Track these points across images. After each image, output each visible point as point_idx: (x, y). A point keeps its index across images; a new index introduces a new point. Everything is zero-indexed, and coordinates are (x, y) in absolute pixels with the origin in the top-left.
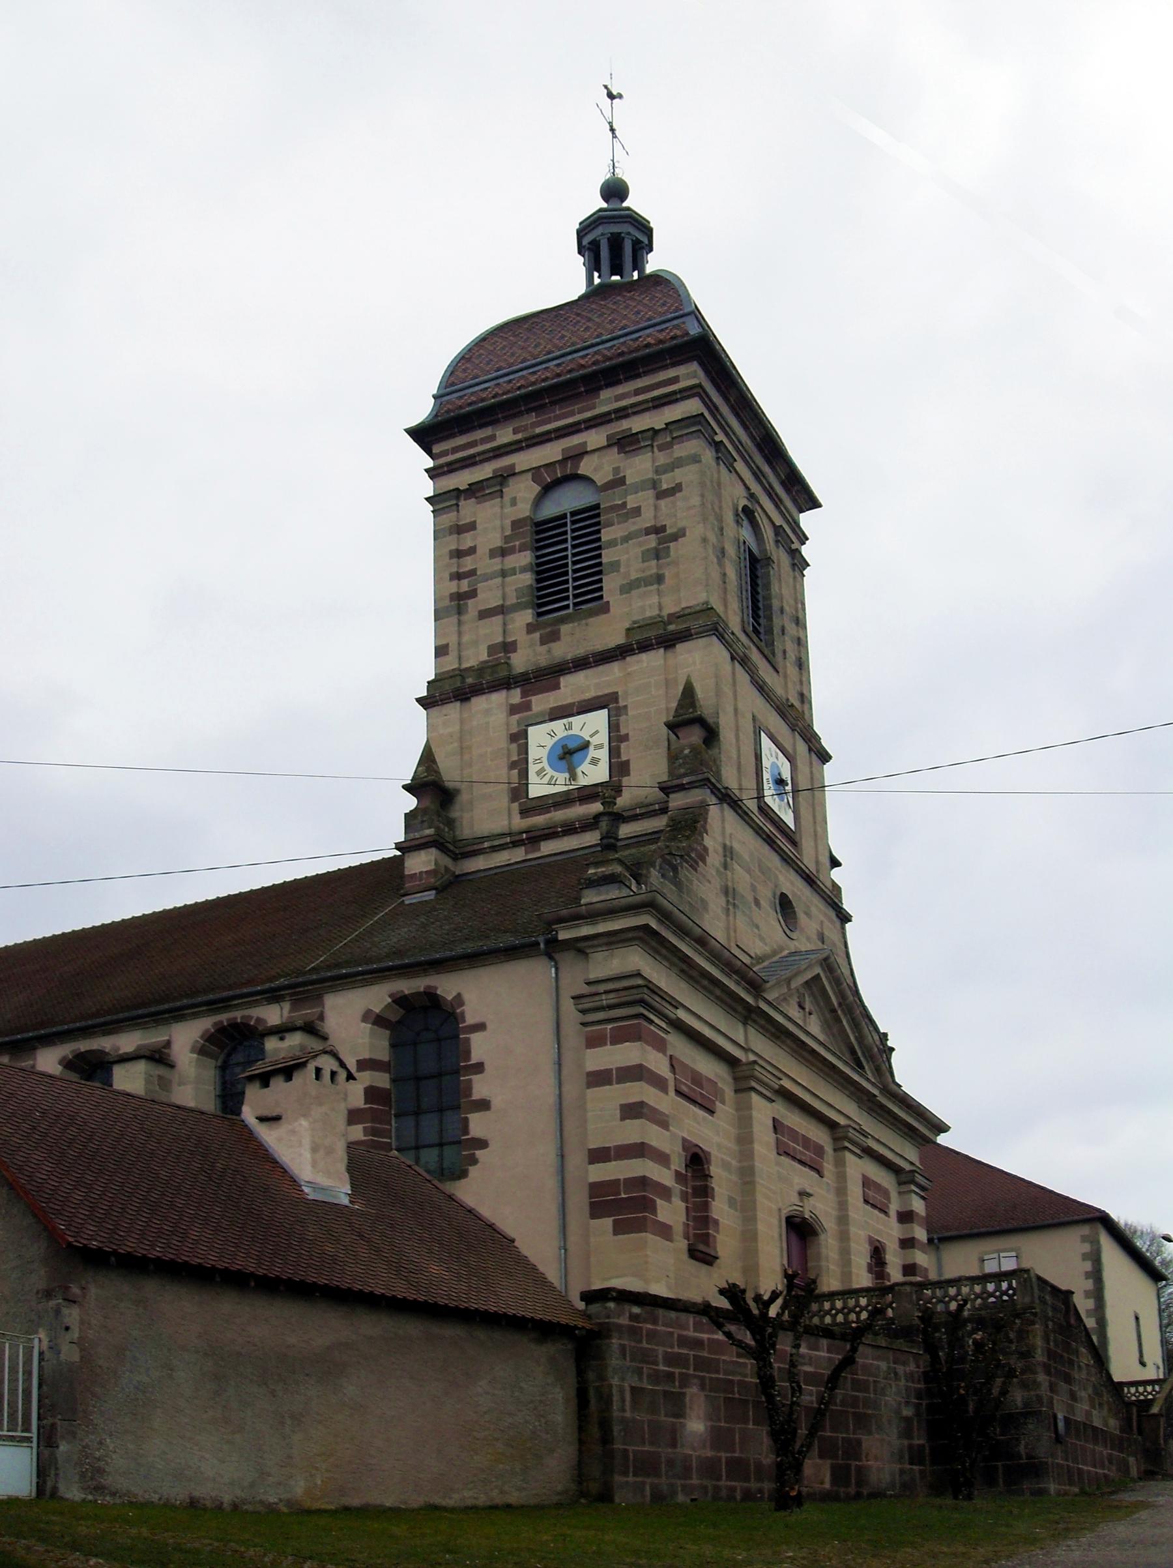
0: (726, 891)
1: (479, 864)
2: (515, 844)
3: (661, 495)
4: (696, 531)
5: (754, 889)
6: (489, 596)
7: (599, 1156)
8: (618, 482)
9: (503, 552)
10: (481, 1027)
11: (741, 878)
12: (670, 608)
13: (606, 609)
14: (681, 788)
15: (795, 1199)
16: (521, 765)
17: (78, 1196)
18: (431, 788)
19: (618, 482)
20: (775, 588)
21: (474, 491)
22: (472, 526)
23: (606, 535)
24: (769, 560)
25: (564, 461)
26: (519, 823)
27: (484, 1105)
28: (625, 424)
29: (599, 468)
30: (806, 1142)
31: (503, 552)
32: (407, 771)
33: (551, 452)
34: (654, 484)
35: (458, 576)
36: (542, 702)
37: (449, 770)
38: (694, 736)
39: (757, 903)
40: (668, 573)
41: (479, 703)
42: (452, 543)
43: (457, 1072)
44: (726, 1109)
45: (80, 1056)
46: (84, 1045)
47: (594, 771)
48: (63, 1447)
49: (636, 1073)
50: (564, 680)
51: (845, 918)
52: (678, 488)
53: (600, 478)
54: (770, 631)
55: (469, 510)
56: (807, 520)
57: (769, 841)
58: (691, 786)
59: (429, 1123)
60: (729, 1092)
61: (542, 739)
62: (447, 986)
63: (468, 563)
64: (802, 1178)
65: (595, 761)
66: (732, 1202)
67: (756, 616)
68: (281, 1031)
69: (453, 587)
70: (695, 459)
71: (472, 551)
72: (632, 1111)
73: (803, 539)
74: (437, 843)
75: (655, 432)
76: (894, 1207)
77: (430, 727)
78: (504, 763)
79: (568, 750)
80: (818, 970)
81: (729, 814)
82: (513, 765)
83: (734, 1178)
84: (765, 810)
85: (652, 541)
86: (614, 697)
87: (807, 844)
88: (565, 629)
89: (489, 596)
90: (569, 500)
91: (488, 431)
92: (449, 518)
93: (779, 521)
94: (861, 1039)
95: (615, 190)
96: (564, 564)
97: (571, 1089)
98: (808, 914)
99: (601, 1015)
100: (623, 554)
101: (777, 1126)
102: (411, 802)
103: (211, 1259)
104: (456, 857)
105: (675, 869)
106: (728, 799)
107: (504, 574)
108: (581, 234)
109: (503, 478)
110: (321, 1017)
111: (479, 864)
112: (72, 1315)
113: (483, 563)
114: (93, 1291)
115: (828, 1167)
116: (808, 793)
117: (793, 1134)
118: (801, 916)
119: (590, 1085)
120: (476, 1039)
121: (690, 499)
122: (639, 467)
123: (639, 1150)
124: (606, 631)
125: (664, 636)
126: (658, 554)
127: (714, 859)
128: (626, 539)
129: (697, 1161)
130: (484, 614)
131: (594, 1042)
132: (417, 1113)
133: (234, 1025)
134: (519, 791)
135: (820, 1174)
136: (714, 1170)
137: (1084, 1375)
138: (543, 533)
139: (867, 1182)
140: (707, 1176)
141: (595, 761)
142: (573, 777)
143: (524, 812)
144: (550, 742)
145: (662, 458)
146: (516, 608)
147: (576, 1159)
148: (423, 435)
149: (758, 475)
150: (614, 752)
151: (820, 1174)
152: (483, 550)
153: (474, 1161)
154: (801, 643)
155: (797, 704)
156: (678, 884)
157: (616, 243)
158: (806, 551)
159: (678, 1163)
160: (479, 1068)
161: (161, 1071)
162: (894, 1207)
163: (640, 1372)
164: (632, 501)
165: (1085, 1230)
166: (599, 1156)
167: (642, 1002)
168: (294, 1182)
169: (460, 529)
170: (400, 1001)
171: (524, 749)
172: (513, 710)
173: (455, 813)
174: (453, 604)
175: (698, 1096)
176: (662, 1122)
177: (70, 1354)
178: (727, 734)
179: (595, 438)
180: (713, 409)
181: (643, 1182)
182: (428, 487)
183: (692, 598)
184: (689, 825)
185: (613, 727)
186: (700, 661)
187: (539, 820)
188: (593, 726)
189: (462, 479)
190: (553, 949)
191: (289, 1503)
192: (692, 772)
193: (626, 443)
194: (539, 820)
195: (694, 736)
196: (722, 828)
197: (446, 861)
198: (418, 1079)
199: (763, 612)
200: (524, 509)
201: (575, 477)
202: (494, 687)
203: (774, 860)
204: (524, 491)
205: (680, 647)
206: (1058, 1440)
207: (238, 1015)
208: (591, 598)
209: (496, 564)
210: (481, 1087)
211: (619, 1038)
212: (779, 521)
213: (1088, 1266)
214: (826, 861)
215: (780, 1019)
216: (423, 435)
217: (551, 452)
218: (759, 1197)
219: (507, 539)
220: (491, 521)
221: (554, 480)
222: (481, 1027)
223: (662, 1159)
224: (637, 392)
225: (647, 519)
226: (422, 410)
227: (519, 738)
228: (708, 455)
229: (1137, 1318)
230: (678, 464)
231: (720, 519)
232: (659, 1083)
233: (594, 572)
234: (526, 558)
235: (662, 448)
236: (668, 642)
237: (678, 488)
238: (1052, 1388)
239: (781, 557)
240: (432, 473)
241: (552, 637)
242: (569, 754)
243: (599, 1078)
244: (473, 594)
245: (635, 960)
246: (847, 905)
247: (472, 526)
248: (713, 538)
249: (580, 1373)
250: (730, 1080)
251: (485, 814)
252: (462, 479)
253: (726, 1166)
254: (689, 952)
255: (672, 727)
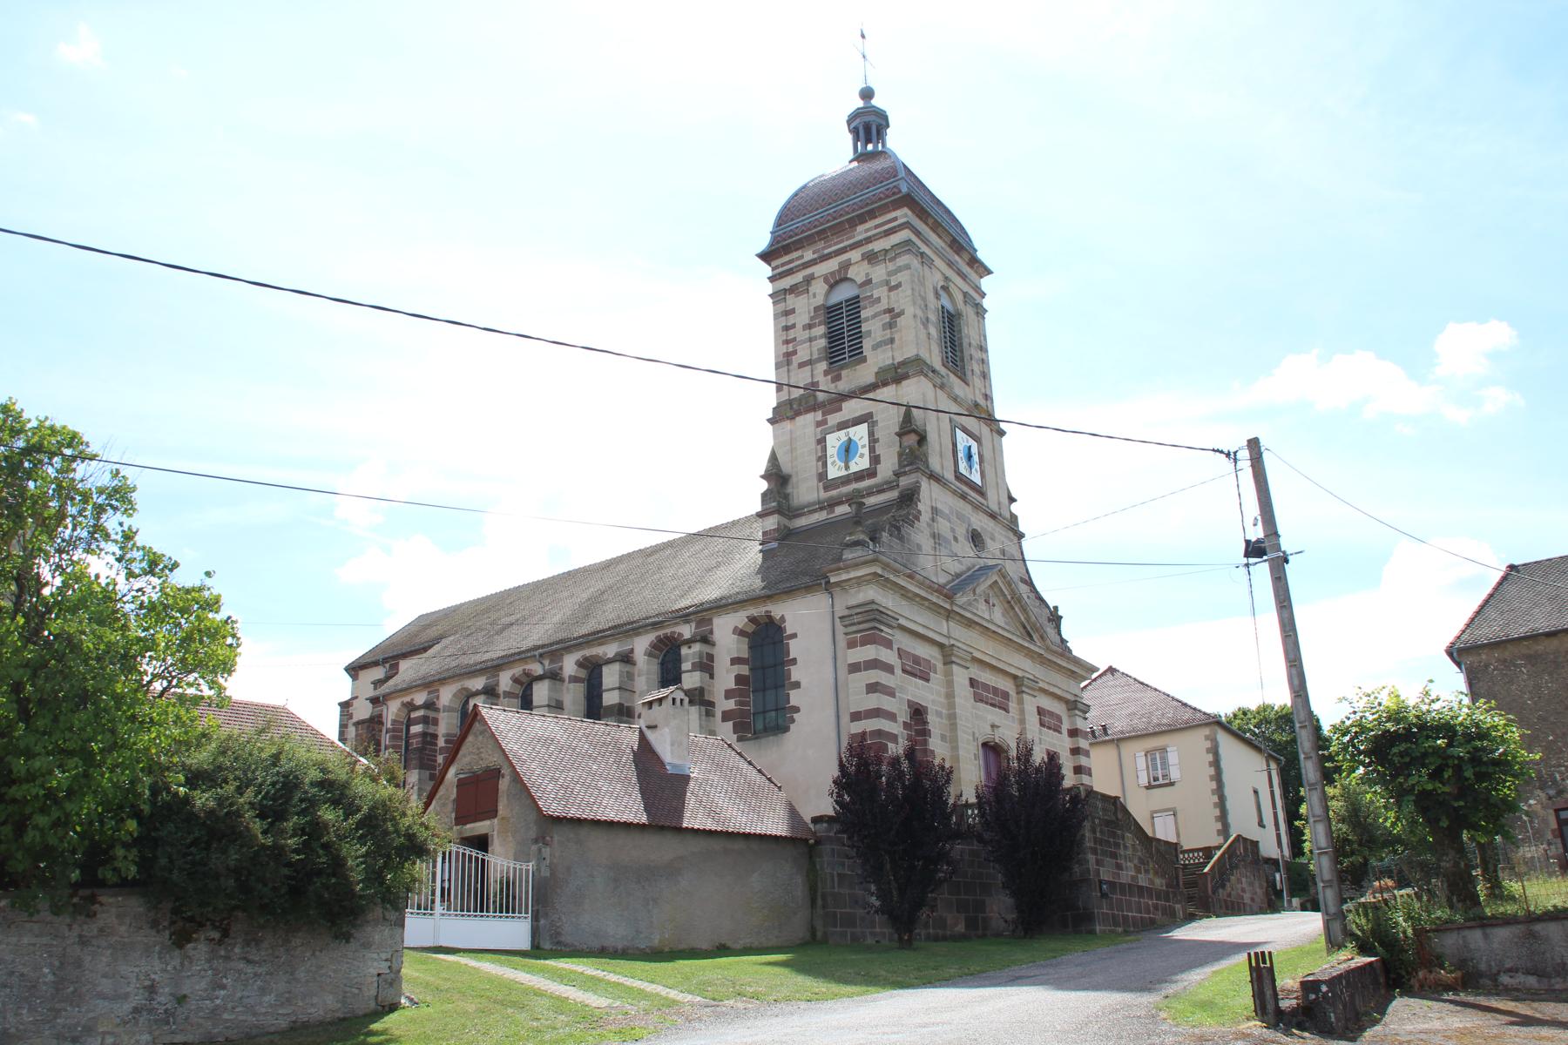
0: (934, 536)
1: (802, 522)
2: (821, 509)
3: (892, 289)
4: (910, 311)
5: (953, 530)
6: (803, 354)
7: (856, 717)
8: (868, 282)
9: (809, 327)
10: (794, 636)
11: (943, 526)
12: (899, 359)
13: (864, 360)
14: (905, 473)
15: (988, 730)
16: (823, 459)
17: (550, 787)
18: (777, 477)
19: (868, 282)
20: (965, 331)
21: (793, 290)
22: (793, 311)
23: (864, 314)
24: (959, 315)
25: (839, 271)
26: (823, 495)
27: (797, 685)
28: (870, 247)
29: (858, 273)
30: (995, 691)
31: (809, 327)
32: (762, 465)
33: (832, 265)
34: (887, 283)
35: (787, 342)
36: (834, 419)
37: (786, 468)
38: (911, 440)
39: (956, 539)
40: (896, 337)
41: (800, 420)
42: (783, 322)
43: (783, 664)
44: (937, 677)
45: (586, 659)
46: (588, 652)
47: (861, 463)
48: (542, 922)
49: (874, 664)
50: (845, 405)
51: (1021, 536)
52: (899, 285)
53: (860, 280)
54: (962, 360)
55: (792, 301)
56: (985, 283)
57: (964, 497)
58: (911, 472)
59: (770, 694)
60: (940, 666)
61: (834, 441)
62: (777, 610)
63: (792, 334)
64: (994, 715)
65: (862, 456)
66: (943, 738)
67: (954, 350)
68: (689, 642)
69: (784, 349)
70: (908, 267)
71: (794, 326)
72: (873, 688)
73: (983, 295)
74: (778, 511)
75: (886, 251)
76: (1065, 727)
77: (775, 437)
78: (814, 458)
79: (851, 450)
80: (995, 578)
81: (934, 485)
82: (819, 459)
83: (945, 721)
84: (959, 477)
85: (887, 318)
86: (870, 415)
87: (991, 494)
88: (844, 373)
89: (803, 354)
90: (843, 293)
91: (799, 253)
92: (782, 307)
93: (966, 288)
94: (1028, 619)
95: (867, 94)
96: (842, 332)
97: (843, 670)
98: (993, 539)
99: (854, 628)
100: (873, 327)
101: (973, 683)
102: (764, 485)
103: (611, 815)
104: (790, 519)
105: (898, 529)
106: (934, 477)
107: (811, 340)
108: (849, 122)
109: (809, 280)
110: (711, 632)
111: (802, 522)
112: (546, 851)
113: (799, 333)
114: (556, 838)
115: (1013, 705)
116: (992, 462)
117: (986, 687)
118: (988, 542)
119: (851, 672)
120: (792, 642)
121: (906, 291)
122: (879, 272)
123: (876, 713)
124: (864, 374)
125: (895, 375)
126: (891, 325)
127: (925, 517)
128: (874, 316)
129: (918, 713)
130: (801, 365)
131: (851, 645)
132: (764, 690)
133: (666, 637)
134: (822, 476)
135: (1007, 711)
136: (931, 718)
137: (1129, 852)
138: (831, 314)
139: (1040, 711)
140: (925, 723)
141: (862, 456)
142: (847, 468)
143: (826, 488)
144: (838, 444)
145: (891, 267)
146: (819, 360)
147: (845, 718)
148: (766, 256)
149: (950, 264)
150: (872, 449)
151: (1007, 711)
152: (799, 326)
153: (793, 721)
154: (984, 362)
155: (982, 402)
156: (901, 538)
157: (867, 128)
158: (986, 303)
159: (904, 716)
160: (794, 661)
161: (628, 668)
162: (1065, 727)
163: (843, 865)
164: (876, 294)
165: (1207, 731)
166: (856, 717)
167: (874, 620)
168: (662, 764)
169: (787, 313)
170: (752, 620)
171: (824, 449)
172: (819, 424)
173: (789, 490)
174: (785, 360)
175: (917, 670)
176: (890, 692)
177: (546, 873)
178: (932, 436)
179: (855, 255)
180: (918, 233)
181: (879, 733)
182: (769, 288)
183: (909, 352)
184: (909, 498)
185: (871, 434)
186: (914, 390)
187: (834, 493)
188: (860, 433)
189: (787, 282)
190: (829, 587)
191: (651, 948)
192: (911, 464)
193: (871, 258)
194: (834, 493)
195: (911, 440)
196: (930, 495)
197: (785, 521)
198: (763, 668)
199: (958, 343)
200: (819, 300)
201: (846, 279)
202: (808, 411)
203: (967, 509)
204: (819, 288)
205: (905, 383)
206: (1104, 895)
207: (668, 631)
208: (858, 355)
209: (806, 335)
210: (796, 674)
211: (865, 642)
212: (966, 288)
213: (1210, 757)
214: (1005, 501)
215: (968, 615)
216: (766, 256)
217: (832, 265)
218: (959, 733)
219: (812, 318)
220: (804, 308)
221: (835, 281)
222: (794, 636)
223: (892, 717)
224: (876, 227)
225: (884, 305)
226: (763, 241)
227: (822, 441)
228: (915, 262)
229: (1256, 792)
230: (899, 270)
231: (924, 299)
232: (889, 669)
233: (858, 336)
234: (821, 330)
235: (891, 260)
236: (898, 380)
237: (899, 285)
238: (1098, 862)
239: (968, 312)
240: (772, 279)
241: (837, 378)
242: (848, 450)
243: (855, 668)
244: (795, 353)
245: (870, 593)
246: (1022, 529)
247: (793, 311)
248: (919, 313)
249: (812, 863)
250: (940, 657)
251: (806, 491)
252: (787, 282)
253: (939, 714)
254: (902, 583)
255: (900, 435)
